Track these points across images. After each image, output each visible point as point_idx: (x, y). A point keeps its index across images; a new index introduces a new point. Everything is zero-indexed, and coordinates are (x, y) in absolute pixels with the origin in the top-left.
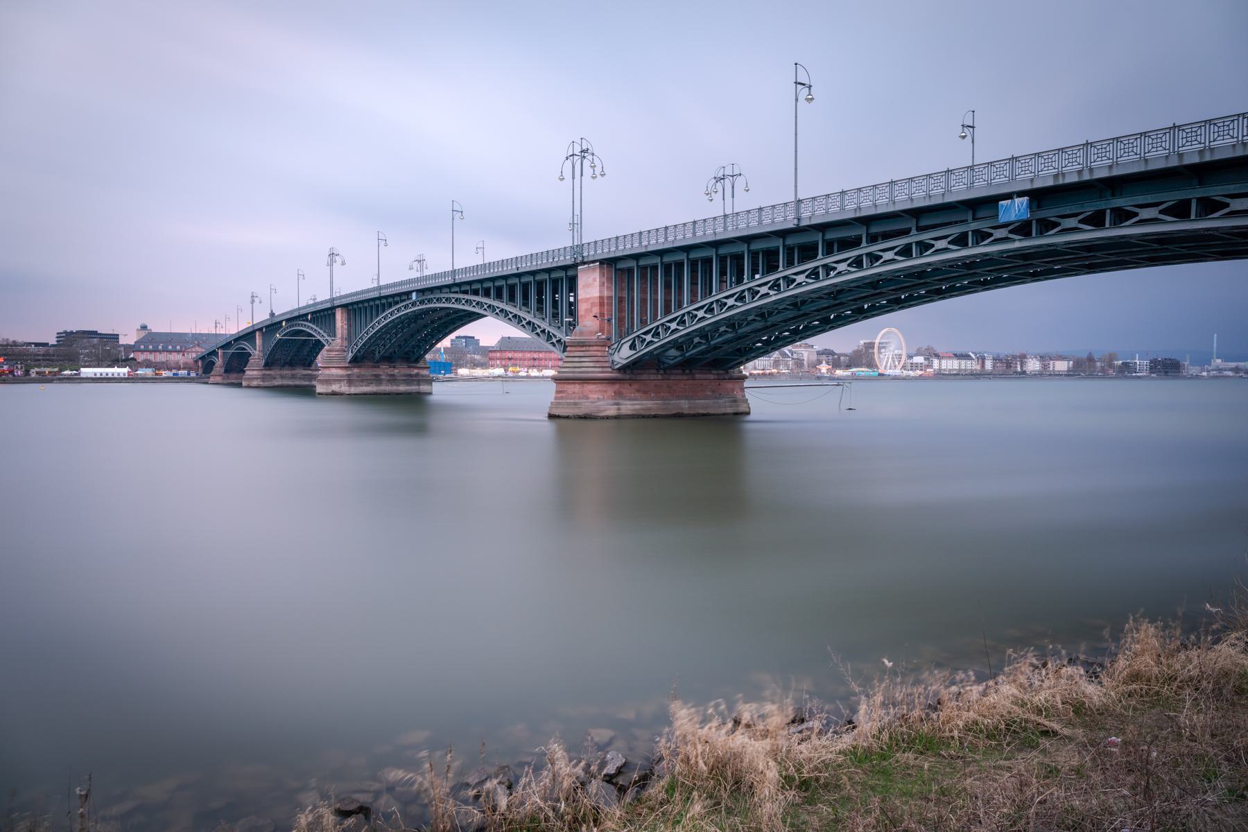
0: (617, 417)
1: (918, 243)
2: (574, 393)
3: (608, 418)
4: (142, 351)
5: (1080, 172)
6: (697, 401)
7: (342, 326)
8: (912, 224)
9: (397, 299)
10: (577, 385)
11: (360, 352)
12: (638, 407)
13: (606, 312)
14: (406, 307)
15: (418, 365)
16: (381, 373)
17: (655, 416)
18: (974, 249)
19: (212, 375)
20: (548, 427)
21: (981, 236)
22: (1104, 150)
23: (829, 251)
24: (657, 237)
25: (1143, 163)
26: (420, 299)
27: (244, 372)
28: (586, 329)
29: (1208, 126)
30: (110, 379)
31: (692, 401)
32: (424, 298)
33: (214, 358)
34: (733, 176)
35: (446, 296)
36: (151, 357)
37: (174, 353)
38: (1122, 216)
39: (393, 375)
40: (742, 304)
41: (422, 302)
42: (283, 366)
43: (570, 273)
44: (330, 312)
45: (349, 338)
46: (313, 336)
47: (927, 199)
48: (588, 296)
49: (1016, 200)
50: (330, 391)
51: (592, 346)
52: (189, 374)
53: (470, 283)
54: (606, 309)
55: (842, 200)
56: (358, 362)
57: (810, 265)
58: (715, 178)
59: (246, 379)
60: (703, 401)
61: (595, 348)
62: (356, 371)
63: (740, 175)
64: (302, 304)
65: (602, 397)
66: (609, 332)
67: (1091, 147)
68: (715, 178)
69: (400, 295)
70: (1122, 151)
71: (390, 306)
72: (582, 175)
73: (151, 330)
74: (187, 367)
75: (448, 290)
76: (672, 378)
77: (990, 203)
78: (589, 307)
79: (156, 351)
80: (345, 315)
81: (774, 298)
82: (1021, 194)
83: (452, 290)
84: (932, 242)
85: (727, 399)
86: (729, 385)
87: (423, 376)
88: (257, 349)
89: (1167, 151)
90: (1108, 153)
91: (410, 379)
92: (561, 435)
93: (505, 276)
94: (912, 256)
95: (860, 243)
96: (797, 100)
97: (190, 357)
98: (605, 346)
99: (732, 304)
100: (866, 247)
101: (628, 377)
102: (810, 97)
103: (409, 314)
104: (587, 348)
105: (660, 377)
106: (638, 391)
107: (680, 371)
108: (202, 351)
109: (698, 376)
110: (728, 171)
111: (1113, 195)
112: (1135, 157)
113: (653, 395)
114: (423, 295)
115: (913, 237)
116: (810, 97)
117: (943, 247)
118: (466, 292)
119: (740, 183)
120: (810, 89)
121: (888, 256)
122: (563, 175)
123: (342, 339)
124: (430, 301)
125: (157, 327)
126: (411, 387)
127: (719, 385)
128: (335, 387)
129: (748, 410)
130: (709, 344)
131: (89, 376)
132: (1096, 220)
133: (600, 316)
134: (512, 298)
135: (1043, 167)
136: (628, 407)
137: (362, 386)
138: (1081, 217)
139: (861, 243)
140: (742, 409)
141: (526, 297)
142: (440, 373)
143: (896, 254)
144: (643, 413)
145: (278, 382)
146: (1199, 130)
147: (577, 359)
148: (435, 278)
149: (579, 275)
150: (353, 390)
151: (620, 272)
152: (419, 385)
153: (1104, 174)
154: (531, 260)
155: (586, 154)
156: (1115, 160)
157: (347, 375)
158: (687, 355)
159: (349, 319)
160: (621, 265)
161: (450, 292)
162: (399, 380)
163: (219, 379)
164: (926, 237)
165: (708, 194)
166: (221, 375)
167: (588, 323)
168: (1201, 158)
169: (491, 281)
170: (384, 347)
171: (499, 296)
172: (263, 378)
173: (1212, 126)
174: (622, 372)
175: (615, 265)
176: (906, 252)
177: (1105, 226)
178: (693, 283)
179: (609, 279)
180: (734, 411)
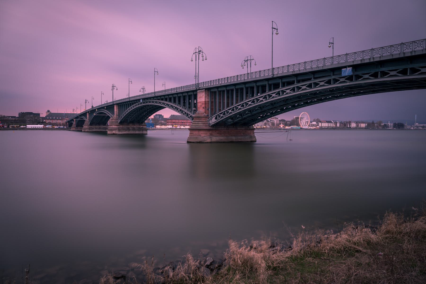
0: (211, 143)
2: (196, 134)
3: (207, 143)
4: (48, 119)
5: (370, 59)
6: (238, 137)
9: (135, 102)
10: (197, 131)
11: (123, 120)
12: (218, 139)
13: (207, 107)
14: (138, 104)
15: (143, 124)
16: (130, 127)
17: (224, 142)
18: (381, 79)
19: (72, 128)
20: (187, 146)
21: (336, 81)
23: (283, 86)
26: (143, 102)
27: (83, 126)
28: (200, 112)
32: (145, 101)
33: (73, 122)
34: (251, 60)
35: (152, 101)
36: (51, 121)
38: (384, 74)
39: (134, 128)
41: (144, 103)
42: (96, 125)
43: (195, 93)
45: (119, 115)
47: (317, 68)
48: (201, 101)
49: (348, 68)
50: (112, 133)
51: (202, 118)
52: (64, 127)
53: (160, 96)
54: (207, 106)
57: (277, 91)
58: (244, 60)
61: (203, 119)
62: (121, 126)
63: (253, 59)
64: (103, 103)
66: (208, 113)
68: (244, 60)
69: (136, 100)
70: (365, 55)
71: (133, 104)
72: (199, 59)
73: (51, 112)
74: (63, 125)
78: (201, 105)
79: (52, 119)
80: (118, 107)
81: (264, 102)
82: (349, 66)
83: (154, 99)
84: (319, 83)
86: (249, 132)
87: (144, 128)
88: (87, 119)
91: (140, 129)
94: (312, 87)
95: (294, 83)
96: (273, 34)
97: (64, 121)
98: (207, 118)
100: (296, 84)
101: (214, 129)
102: (277, 33)
103: (140, 107)
104: (201, 119)
105: (225, 129)
108: (68, 119)
109: (238, 128)
110: (249, 58)
111: (381, 67)
113: (223, 135)
116: (277, 33)
118: (159, 99)
119: (253, 62)
120: (277, 30)
121: (304, 87)
122: (278, 32)
123: (117, 115)
124: (147, 102)
125: (53, 111)
126: (140, 132)
127: (246, 131)
128: (114, 132)
129: (255, 140)
131: (30, 128)
132: (375, 75)
134: (175, 102)
135: (357, 57)
136: (214, 139)
137: (123, 131)
138: (370, 74)
139: (295, 83)
140: (254, 140)
142: (150, 127)
144: (219, 141)
145: (94, 130)
146: (411, 45)
147: (197, 123)
150: (120, 133)
152: (143, 131)
153: (378, 59)
155: (200, 52)
158: (235, 121)
159: (119, 109)
160: (212, 90)
161: (154, 99)
162: (136, 129)
163: (74, 129)
164: (317, 81)
165: (242, 66)
166: (75, 128)
167: (201, 110)
168: (411, 54)
170: (131, 118)
171: (170, 101)
172: (89, 129)
176: (310, 86)
178: (237, 96)
179: (208, 95)
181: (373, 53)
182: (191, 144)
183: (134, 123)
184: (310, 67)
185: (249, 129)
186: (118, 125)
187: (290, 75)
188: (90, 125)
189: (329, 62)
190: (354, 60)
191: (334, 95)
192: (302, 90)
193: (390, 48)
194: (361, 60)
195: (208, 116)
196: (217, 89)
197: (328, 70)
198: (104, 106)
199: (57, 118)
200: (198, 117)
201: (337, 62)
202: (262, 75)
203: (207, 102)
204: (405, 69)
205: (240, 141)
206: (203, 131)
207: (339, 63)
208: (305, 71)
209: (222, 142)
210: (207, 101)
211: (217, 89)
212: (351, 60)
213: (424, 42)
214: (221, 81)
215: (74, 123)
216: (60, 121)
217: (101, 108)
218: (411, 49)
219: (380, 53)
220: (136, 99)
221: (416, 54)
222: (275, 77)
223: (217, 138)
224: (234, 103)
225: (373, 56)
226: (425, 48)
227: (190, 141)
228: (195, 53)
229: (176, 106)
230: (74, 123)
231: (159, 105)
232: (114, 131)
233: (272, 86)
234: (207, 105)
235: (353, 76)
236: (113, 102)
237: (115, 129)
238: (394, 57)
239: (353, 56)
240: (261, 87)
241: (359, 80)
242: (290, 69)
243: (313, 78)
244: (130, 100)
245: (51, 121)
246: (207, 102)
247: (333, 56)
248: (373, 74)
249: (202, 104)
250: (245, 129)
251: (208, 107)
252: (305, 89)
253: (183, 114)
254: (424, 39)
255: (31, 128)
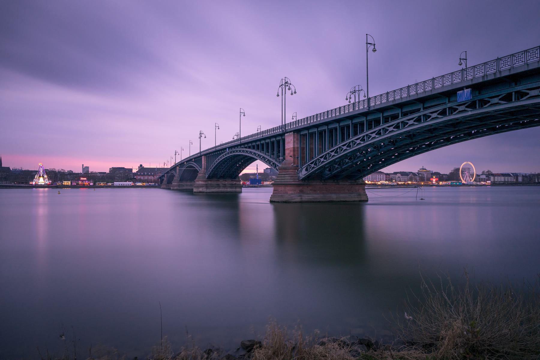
0: (301, 202)
1: (424, 115)
2: (281, 191)
4: (139, 175)
5: (495, 74)
6: (340, 195)
7: (204, 164)
8: (421, 106)
10: (282, 187)
12: (310, 197)
14: (226, 155)
15: (236, 180)
16: (220, 183)
17: (319, 202)
18: (516, 102)
20: (270, 207)
21: (452, 110)
22: (506, 61)
24: (324, 116)
25: (526, 66)
27: (172, 183)
28: (287, 162)
29: (526, 53)
30: (123, 186)
31: (338, 195)
35: (239, 149)
36: (142, 178)
37: (151, 176)
38: (521, 95)
39: (225, 184)
40: (349, 148)
41: (231, 152)
44: (279, 138)
46: (195, 168)
48: (289, 147)
50: (198, 191)
51: (290, 169)
52: (155, 184)
53: (247, 143)
55: (433, 84)
56: (210, 179)
57: (378, 129)
59: (195, 187)
60: (343, 195)
61: (291, 170)
62: (209, 182)
65: (294, 193)
66: (298, 163)
67: (500, 60)
69: (221, 150)
70: (530, 57)
72: (285, 94)
74: (155, 181)
75: (240, 147)
76: (328, 184)
77: (451, 94)
78: (289, 152)
79: (144, 175)
80: (205, 159)
81: (362, 145)
82: (467, 87)
83: (241, 147)
84: (430, 114)
85: (356, 194)
86: (357, 187)
87: (238, 184)
88: (177, 174)
89: (495, 70)
90: (508, 63)
91: (232, 186)
92: (276, 210)
93: (326, 122)
94: (446, 115)
95: (398, 117)
97: (156, 177)
99: (345, 149)
100: (401, 118)
101: (306, 183)
102: (375, 49)
103: (228, 158)
104: (288, 170)
105: (322, 184)
106: (311, 190)
107: (332, 181)
109: (341, 183)
112: (522, 63)
113: (318, 192)
114: (232, 149)
115: (422, 112)
116: (375, 49)
117: (435, 117)
120: (374, 46)
121: (411, 122)
122: (375, 48)
124: (234, 152)
125: (146, 166)
127: (352, 187)
128: (201, 190)
129: (366, 199)
130: (342, 168)
131: (117, 185)
132: (508, 98)
133: (293, 156)
134: (263, 150)
137: (212, 189)
138: (500, 97)
140: (363, 198)
141: (273, 150)
142: (257, 184)
143: (438, 114)
144: (313, 200)
145: (185, 188)
147: (283, 176)
148: (275, 130)
149: (285, 138)
151: (303, 136)
152: (236, 188)
153: (507, 74)
154: (310, 119)
156: (512, 66)
157: (206, 184)
160: (302, 133)
161: (241, 148)
162: (227, 186)
163: (165, 186)
164: (427, 112)
166: (166, 185)
168: (472, 83)
169: (269, 139)
171: (254, 148)
172: (179, 186)
173: (528, 53)
174: (304, 181)
175: (300, 133)
176: (418, 120)
177: (512, 101)
179: (297, 139)
180: (359, 200)
181: (486, 69)
182: (276, 203)
183: (225, 179)
184: (450, 83)
185: (356, 185)
186: (206, 181)
187: (342, 118)
188: (179, 181)
189: (481, 72)
190: (472, 77)
191: (519, 121)
192: (409, 126)
193: (524, 54)
194: (483, 77)
195: (298, 166)
196: (327, 126)
197: (393, 107)
198: (183, 161)
199: (150, 174)
200: (285, 169)
201: (472, 76)
202: (391, 99)
203: (296, 148)
204: (508, 93)
205: (342, 200)
206: (290, 186)
207: (475, 77)
208: (408, 99)
209: (317, 201)
210: (297, 147)
211: (327, 126)
212: (448, 84)
213: (525, 54)
214: (335, 113)
215: (165, 179)
216: (152, 178)
217: (189, 160)
218: (538, 58)
219: (472, 74)
220: (255, 140)
221: (503, 75)
222: (371, 110)
223: (310, 196)
224: (327, 149)
225: (500, 68)
226: (526, 62)
227: (274, 200)
228: (281, 86)
229: (263, 155)
230: (165, 179)
231: (249, 155)
232: (200, 189)
233: (373, 123)
234: (296, 152)
235: (512, 94)
236: (200, 152)
237: (202, 186)
238: (531, 68)
239: (494, 65)
240: (359, 126)
241: (522, 99)
242: (389, 97)
243: (422, 108)
244: (242, 143)
245: (142, 178)
246: (296, 148)
247: (466, 66)
248: (505, 96)
249: (291, 151)
250: (350, 183)
251: (297, 155)
252: (413, 125)
253: (271, 164)
254: (510, 54)
255: (119, 185)
